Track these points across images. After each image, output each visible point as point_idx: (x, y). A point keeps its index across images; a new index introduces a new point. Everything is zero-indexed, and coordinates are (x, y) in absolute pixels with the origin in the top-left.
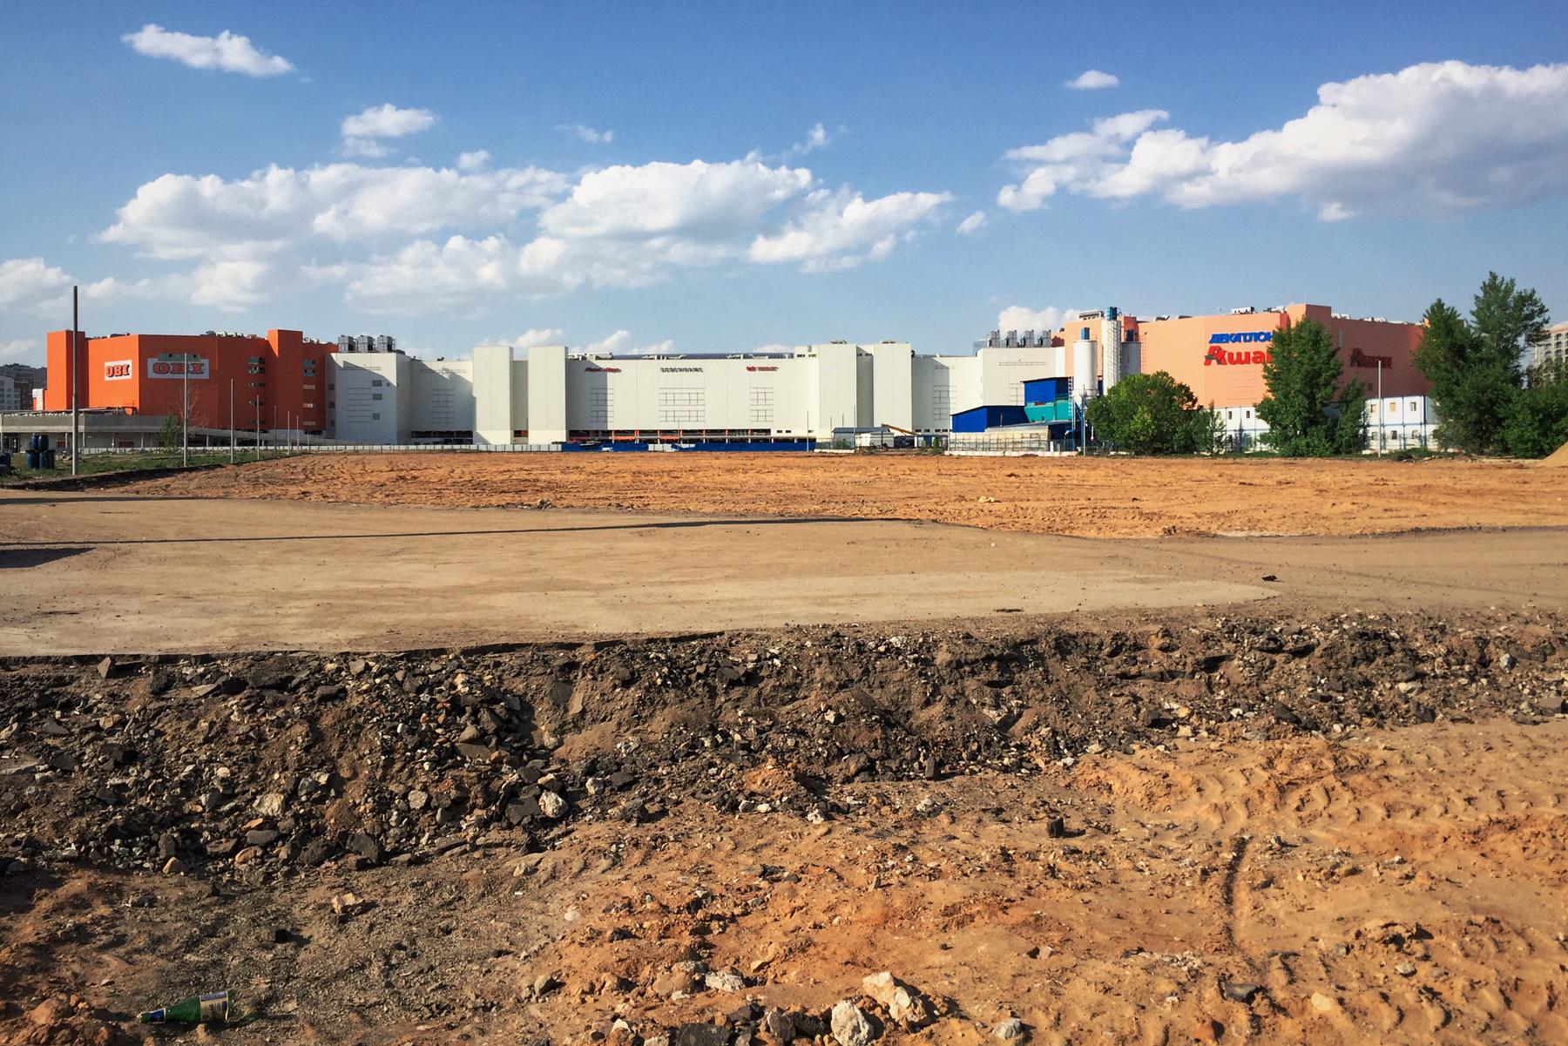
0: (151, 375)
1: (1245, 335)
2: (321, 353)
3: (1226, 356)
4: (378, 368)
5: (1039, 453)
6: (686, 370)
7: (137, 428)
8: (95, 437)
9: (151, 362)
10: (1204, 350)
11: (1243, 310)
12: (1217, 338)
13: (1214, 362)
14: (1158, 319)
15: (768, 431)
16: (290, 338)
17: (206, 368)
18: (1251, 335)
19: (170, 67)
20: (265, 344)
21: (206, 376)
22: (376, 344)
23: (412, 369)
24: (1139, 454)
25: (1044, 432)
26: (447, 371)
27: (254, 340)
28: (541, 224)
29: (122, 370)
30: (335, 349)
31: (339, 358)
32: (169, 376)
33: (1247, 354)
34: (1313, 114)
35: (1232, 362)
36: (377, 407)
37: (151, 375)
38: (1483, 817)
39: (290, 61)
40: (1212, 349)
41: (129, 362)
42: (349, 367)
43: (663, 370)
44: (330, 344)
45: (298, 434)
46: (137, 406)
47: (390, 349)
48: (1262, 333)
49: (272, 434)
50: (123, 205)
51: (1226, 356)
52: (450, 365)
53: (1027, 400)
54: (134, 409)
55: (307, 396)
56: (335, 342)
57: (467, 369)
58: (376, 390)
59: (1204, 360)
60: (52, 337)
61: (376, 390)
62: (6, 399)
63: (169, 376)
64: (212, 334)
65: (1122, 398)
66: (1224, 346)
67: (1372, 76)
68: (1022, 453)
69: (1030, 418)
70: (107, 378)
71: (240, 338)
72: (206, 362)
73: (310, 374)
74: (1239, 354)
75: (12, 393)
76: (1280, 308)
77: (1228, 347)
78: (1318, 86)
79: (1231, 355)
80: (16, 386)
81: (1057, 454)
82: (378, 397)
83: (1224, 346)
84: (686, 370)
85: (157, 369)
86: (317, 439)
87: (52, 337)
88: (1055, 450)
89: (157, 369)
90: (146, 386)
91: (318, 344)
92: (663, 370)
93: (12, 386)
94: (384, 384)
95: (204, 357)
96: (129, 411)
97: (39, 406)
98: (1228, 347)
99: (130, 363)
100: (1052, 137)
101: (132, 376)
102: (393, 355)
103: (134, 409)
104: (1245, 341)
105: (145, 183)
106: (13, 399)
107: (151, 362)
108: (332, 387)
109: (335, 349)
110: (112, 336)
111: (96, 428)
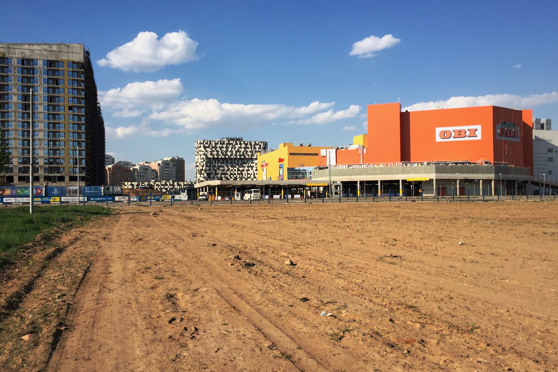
17: (479, 133)
31: (536, 133)
37: (498, 137)
42: (538, 139)
58: (550, 155)
61: (550, 155)
82: (550, 159)
94: (554, 151)
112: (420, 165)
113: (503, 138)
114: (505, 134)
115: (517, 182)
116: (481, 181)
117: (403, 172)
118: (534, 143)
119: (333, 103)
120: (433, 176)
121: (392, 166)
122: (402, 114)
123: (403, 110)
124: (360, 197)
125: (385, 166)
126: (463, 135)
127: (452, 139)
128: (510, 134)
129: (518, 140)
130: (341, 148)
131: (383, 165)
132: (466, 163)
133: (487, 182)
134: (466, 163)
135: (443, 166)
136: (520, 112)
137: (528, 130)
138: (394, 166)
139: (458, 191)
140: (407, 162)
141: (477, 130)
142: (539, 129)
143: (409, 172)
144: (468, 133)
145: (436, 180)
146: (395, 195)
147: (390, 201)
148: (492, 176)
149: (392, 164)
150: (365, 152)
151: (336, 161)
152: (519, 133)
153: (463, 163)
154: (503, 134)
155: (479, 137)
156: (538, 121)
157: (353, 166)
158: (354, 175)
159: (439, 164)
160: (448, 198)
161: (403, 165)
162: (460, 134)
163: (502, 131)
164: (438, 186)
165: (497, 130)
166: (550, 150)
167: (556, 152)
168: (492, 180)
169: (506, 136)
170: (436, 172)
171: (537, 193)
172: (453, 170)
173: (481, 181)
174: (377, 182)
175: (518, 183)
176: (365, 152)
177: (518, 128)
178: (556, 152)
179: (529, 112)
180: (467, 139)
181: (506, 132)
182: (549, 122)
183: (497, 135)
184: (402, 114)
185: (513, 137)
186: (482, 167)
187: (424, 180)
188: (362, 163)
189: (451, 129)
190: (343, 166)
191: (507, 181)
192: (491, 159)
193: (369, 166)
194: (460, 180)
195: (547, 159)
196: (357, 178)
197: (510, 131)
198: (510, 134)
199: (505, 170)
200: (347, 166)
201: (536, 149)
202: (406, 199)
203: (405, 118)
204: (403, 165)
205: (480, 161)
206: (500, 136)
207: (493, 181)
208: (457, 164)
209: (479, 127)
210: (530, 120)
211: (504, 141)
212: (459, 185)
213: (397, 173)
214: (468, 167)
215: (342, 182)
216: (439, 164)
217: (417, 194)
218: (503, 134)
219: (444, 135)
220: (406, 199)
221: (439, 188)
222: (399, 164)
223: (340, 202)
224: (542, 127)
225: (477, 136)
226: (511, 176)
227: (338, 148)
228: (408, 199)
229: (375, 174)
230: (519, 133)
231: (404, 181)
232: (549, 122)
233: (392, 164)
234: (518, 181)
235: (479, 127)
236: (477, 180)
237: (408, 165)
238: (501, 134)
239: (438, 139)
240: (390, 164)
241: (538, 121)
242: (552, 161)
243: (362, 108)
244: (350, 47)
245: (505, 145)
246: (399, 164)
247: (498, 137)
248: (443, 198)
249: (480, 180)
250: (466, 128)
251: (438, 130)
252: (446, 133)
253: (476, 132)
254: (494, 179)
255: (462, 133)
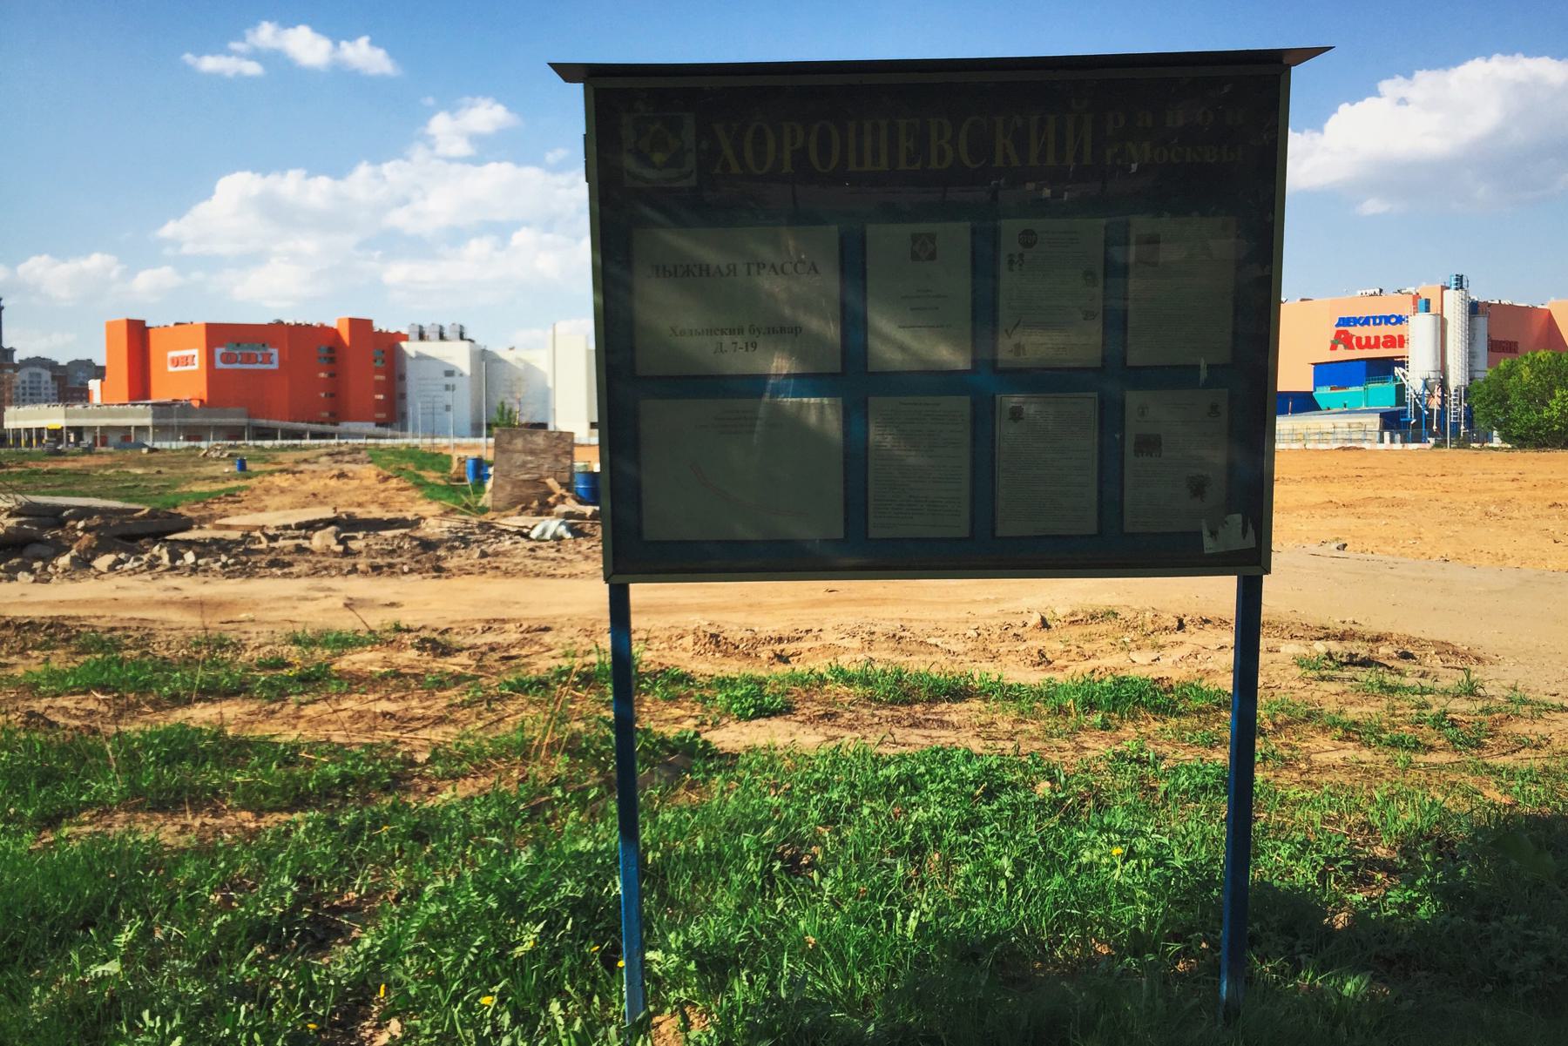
0: (219, 365)
1: (1374, 318)
2: (389, 346)
3: (1354, 341)
4: (450, 358)
5: (1366, 445)
7: (207, 421)
8: (162, 430)
9: (219, 351)
10: (1331, 335)
11: (1372, 292)
12: (1344, 322)
13: (1341, 347)
14: (1302, 300)
16: (360, 326)
17: (275, 358)
18: (1380, 318)
19: (216, 78)
20: (334, 333)
21: (275, 366)
22: (447, 333)
23: (485, 359)
24: (1521, 447)
25: (1374, 422)
26: (520, 360)
27: (324, 329)
28: (1380, 89)
29: (186, 361)
30: (406, 338)
31: (410, 347)
32: (237, 366)
33: (1377, 338)
34: (1370, 102)
36: (448, 397)
37: (219, 365)
39: (392, 54)
40: (1338, 334)
41: (195, 352)
42: (420, 357)
44: (398, 333)
45: (369, 427)
46: (205, 397)
47: (462, 337)
49: (345, 426)
51: (1354, 341)
52: (527, 356)
53: (1317, 383)
54: (202, 401)
55: (379, 387)
56: (404, 331)
57: (540, 360)
58: (449, 381)
59: (1329, 345)
60: (111, 326)
62: (43, 391)
63: (237, 366)
64: (280, 323)
65: (1525, 379)
66: (1351, 330)
67: (1519, 56)
68: (1338, 445)
69: (1322, 406)
70: (171, 369)
71: (309, 326)
72: (275, 351)
73: (379, 364)
74: (1368, 339)
75: (50, 385)
76: (1412, 289)
77: (1356, 331)
78: (1380, 80)
79: (1359, 339)
80: (54, 378)
81: (186, 444)
83: (1351, 330)
85: (226, 358)
86: (389, 432)
87: (111, 326)
88: (1392, 441)
89: (226, 358)
90: (213, 376)
91: (387, 333)
93: (49, 379)
95: (273, 346)
96: (196, 404)
97: (96, 398)
98: (1356, 331)
99: (196, 353)
101: (198, 365)
102: (466, 344)
103: (202, 401)
104: (1375, 324)
106: (50, 392)
107: (219, 351)
108: (402, 377)
109: (406, 338)
110: (177, 324)
111: (163, 421)
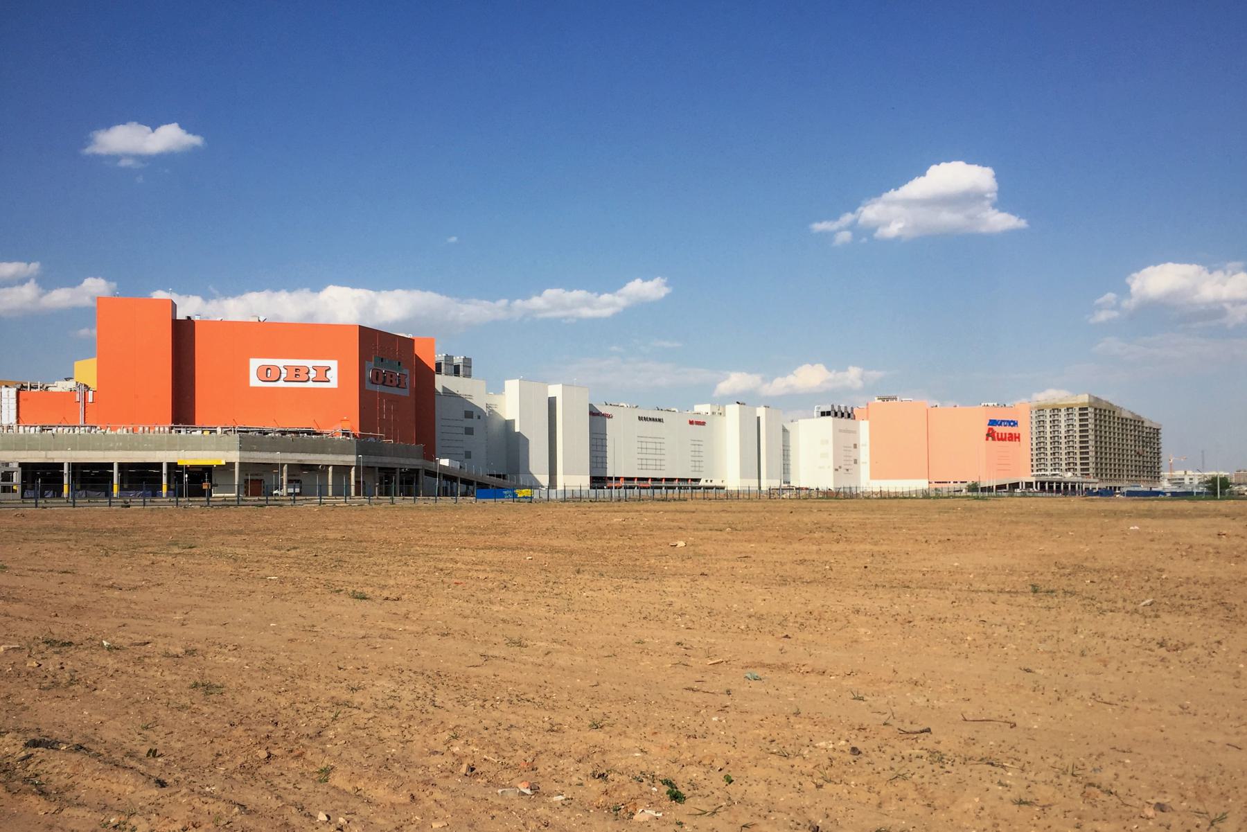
6: (653, 420)
12: (993, 422)
13: (990, 438)
15: (698, 480)
17: (333, 375)
31: (442, 382)
35: (999, 440)
37: (369, 386)
38: (1211, 588)
40: (990, 429)
42: (447, 393)
43: (640, 418)
48: (1012, 421)
50: (1138, 269)
58: (469, 423)
59: (985, 437)
61: (469, 423)
82: (469, 431)
84: (653, 420)
92: (640, 418)
94: (475, 416)
98: (997, 429)
100: (1145, 266)
105: (912, 179)
112: (206, 433)
113: (378, 388)
114: (380, 381)
115: (398, 471)
116: (330, 469)
117: (171, 447)
118: (437, 398)
119: (35, 266)
120: (235, 456)
121: (146, 433)
122: (177, 324)
123: (181, 316)
124: (117, 498)
125: (131, 433)
126: (303, 376)
127: (281, 384)
128: (391, 381)
129: (405, 393)
130: (31, 387)
131: (125, 430)
132: (303, 432)
133: (341, 470)
134: (303, 432)
135: (254, 438)
136: (411, 341)
137: (425, 375)
138: (151, 433)
139: (330, 488)
140: (180, 425)
141: (329, 369)
142: (450, 375)
143: (184, 446)
144: (313, 374)
145: (240, 463)
146: (154, 495)
147: (110, 506)
148: (351, 459)
149: (147, 429)
150: (90, 400)
151: (18, 416)
152: (407, 380)
153: (297, 433)
154: (377, 379)
155: (334, 384)
156: (449, 358)
157: (54, 430)
158: (56, 449)
159: (247, 432)
160: (254, 501)
161: (170, 432)
162: (297, 374)
163: (377, 374)
164: (246, 477)
165: (367, 372)
166: (469, 415)
167: (479, 417)
168: (352, 466)
169: (383, 384)
170: (241, 449)
171: (445, 492)
172: (273, 446)
173: (330, 469)
174: (110, 465)
175: (401, 473)
176: (90, 400)
177: (406, 372)
178: (479, 417)
179: (430, 343)
180: (310, 384)
181: (385, 377)
182: (468, 362)
183: (367, 382)
184: (177, 324)
185: (397, 386)
186: (332, 441)
187: (214, 463)
188: (81, 423)
189: (280, 363)
190: (27, 429)
191: (380, 469)
192: (353, 425)
193: (93, 430)
194: (288, 464)
195: (463, 431)
196: (66, 457)
197: (391, 376)
198: (391, 381)
199: (378, 450)
200: (38, 429)
201: (441, 410)
202: (144, 502)
203: (183, 332)
204: (170, 432)
205: (335, 430)
206: (373, 383)
207: (353, 469)
208: (284, 433)
209: (333, 364)
210: (434, 355)
211: (381, 394)
212: (288, 475)
213: (159, 448)
214: (306, 440)
215: (21, 465)
216: (247, 432)
217: (196, 492)
218: (377, 379)
219: (265, 373)
220: (144, 502)
221: (246, 481)
222: (162, 429)
223: (110, 506)
224: (456, 371)
225: (329, 381)
226: (388, 461)
227: (22, 386)
228: (147, 504)
229: (105, 450)
230: (407, 380)
231: (171, 466)
232: (468, 362)
233: (147, 429)
234: (401, 469)
235: (333, 364)
236: (323, 466)
237: (183, 433)
238: (375, 382)
239: (254, 382)
240: (141, 429)
241: (449, 358)
242: (990, 421)
243: (114, 285)
244: (87, 141)
245: (381, 400)
246: (162, 429)
247: (369, 386)
248: (189, 501)
249: (328, 466)
250: (309, 363)
251: (255, 364)
252: (269, 371)
253: (328, 372)
254: (355, 464)
255: (302, 373)
